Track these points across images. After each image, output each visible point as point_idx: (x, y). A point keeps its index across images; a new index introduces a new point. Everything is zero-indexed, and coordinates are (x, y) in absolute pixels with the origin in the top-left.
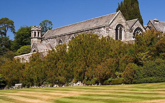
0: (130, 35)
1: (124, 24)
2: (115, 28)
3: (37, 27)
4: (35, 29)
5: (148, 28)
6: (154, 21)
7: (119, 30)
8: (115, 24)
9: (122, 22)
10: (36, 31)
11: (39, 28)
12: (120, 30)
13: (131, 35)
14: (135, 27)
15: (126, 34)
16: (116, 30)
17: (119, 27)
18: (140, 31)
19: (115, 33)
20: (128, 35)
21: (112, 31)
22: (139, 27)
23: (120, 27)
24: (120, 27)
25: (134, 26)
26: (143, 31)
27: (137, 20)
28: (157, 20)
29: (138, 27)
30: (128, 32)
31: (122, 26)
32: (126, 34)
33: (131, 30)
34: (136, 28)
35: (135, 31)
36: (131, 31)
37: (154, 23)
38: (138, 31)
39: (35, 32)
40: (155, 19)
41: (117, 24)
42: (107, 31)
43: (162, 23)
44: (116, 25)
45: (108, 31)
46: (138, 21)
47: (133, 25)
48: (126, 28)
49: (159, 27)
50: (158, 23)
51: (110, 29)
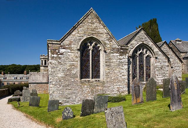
0: (120, 59)
1: (103, 38)
2: (78, 48)
3: (44, 56)
4: (42, 58)
5: (165, 45)
6: (176, 41)
7: (91, 51)
8: (78, 38)
9: (99, 33)
10: (43, 60)
11: (46, 56)
12: (95, 51)
13: (123, 61)
14: (135, 43)
15: (110, 59)
16: (83, 49)
17: (91, 43)
18: (146, 52)
19: (79, 59)
20: (115, 61)
21: (69, 54)
22: (145, 43)
23: (93, 44)
24: (93, 44)
25: (133, 42)
26: (154, 51)
27: (140, 30)
28: (179, 40)
29: (143, 43)
30: (115, 54)
31: (99, 42)
32: (110, 59)
33: (121, 49)
34: (138, 44)
35: (135, 51)
36: (123, 53)
37: (175, 43)
38: (143, 50)
39: (42, 60)
40: (177, 39)
41: (85, 38)
42: (55, 56)
43: (186, 43)
44: (80, 39)
45: (57, 54)
46: (142, 32)
47: (130, 40)
48: (109, 46)
49: (183, 47)
50: (181, 42)
51: (62, 51)
